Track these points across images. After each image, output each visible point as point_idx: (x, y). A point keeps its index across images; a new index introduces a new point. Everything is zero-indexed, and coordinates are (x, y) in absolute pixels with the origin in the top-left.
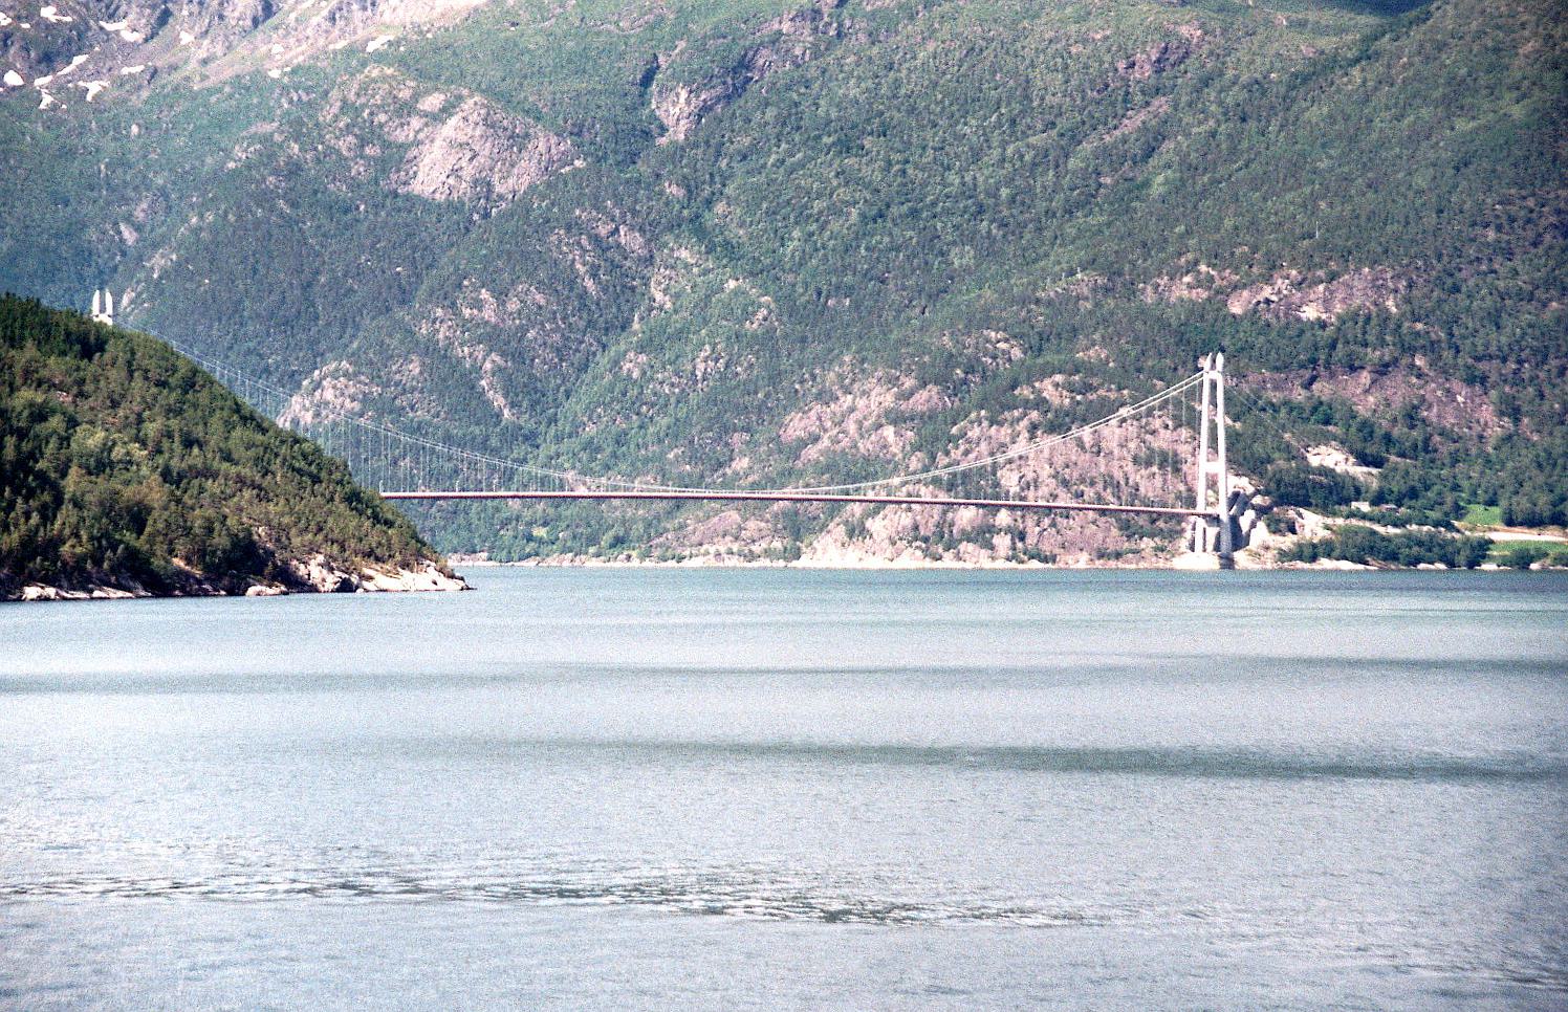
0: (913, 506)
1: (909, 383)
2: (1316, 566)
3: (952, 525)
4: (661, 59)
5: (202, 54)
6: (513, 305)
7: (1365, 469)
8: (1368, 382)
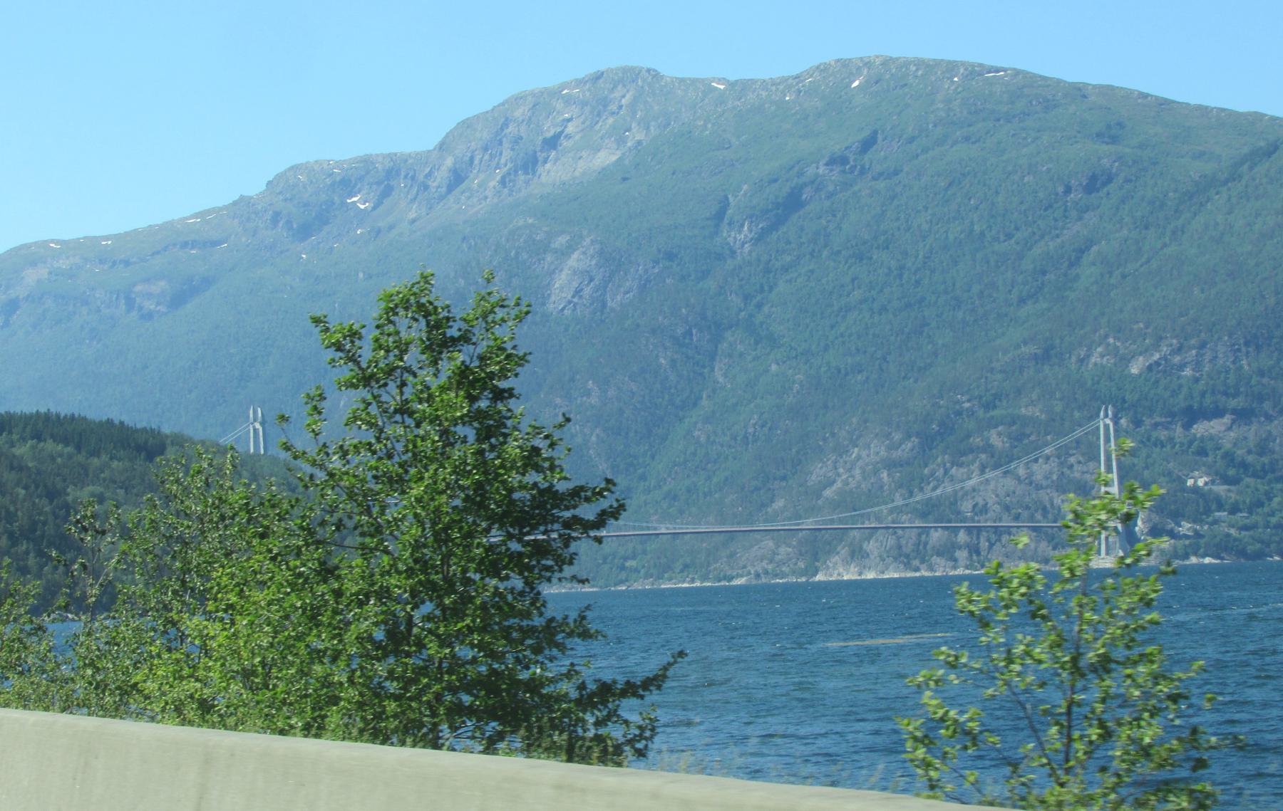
0: (897, 530)
1: (897, 436)
2: (1187, 562)
3: (926, 544)
4: (731, 199)
5: (412, 215)
6: (612, 392)
7: (1226, 487)
8: (1230, 421)
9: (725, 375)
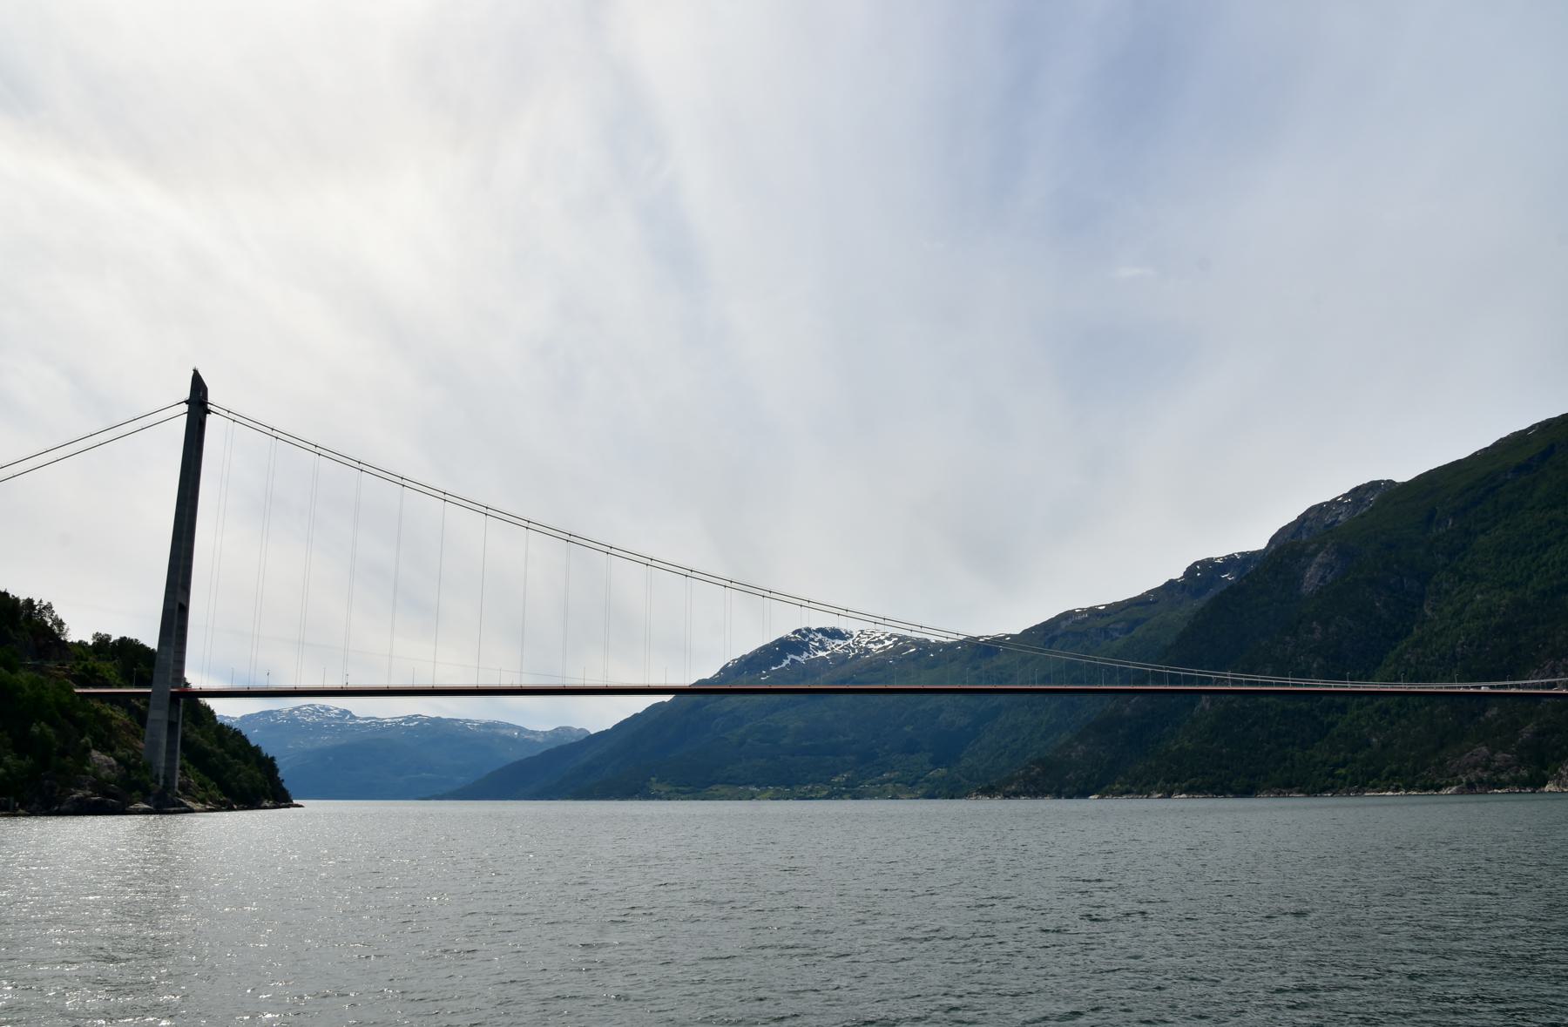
6: (1332, 629)
9: (1433, 610)
